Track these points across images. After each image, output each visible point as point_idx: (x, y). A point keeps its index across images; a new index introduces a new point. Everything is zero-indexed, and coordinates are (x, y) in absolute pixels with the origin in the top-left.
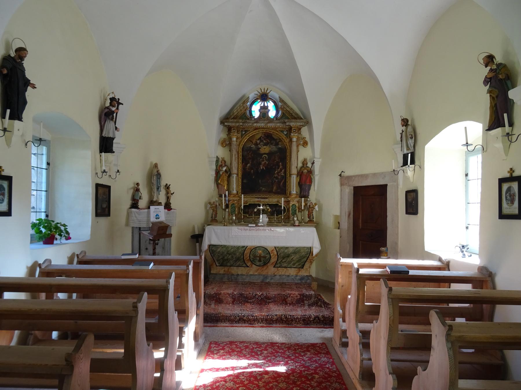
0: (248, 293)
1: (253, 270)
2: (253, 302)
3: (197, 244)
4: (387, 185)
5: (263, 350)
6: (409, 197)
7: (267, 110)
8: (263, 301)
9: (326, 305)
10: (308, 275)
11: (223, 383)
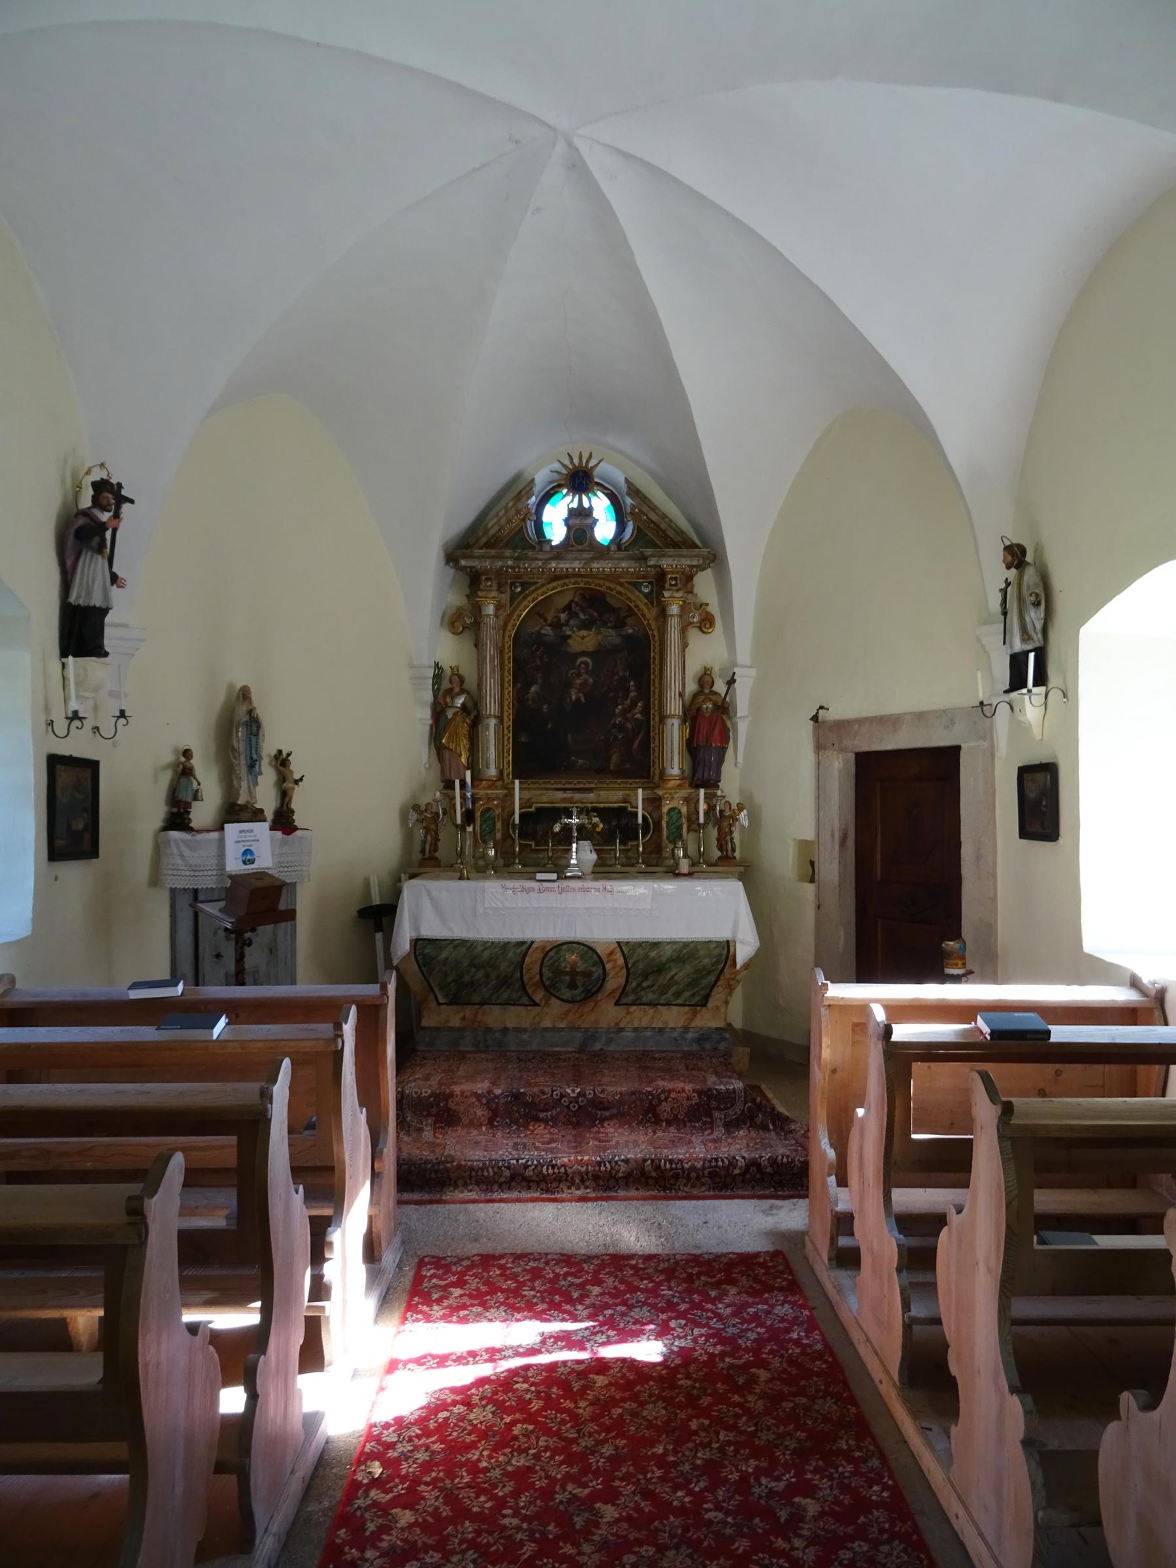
0: (535, 1090)
1: (553, 1014)
2: (555, 1119)
3: (379, 936)
4: (958, 748)
5: (586, 1282)
6: (1028, 784)
7: (588, 521)
8: (585, 1116)
9: (781, 1123)
10: (722, 1025)
11: (459, 1409)
